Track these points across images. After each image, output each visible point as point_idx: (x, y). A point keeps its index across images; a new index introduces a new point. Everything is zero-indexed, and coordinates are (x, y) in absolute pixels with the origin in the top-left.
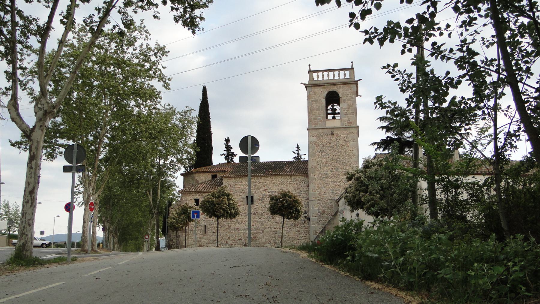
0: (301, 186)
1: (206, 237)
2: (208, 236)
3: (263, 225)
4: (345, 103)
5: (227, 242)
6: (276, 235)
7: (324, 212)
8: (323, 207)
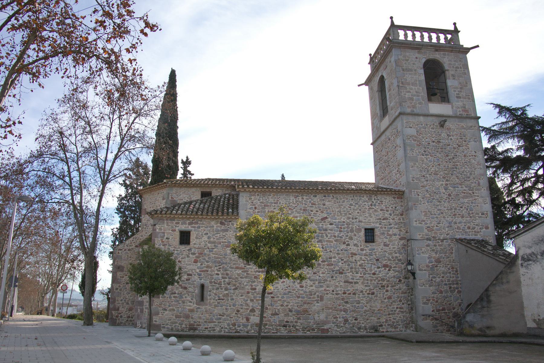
0: (390, 214)
1: (203, 308)
2: (208, 307)
3: (322, 286)
4: (454, 79)
5: (248, 319)
6: (348, 305)
7: (438, 261)
8: (436, 253)
